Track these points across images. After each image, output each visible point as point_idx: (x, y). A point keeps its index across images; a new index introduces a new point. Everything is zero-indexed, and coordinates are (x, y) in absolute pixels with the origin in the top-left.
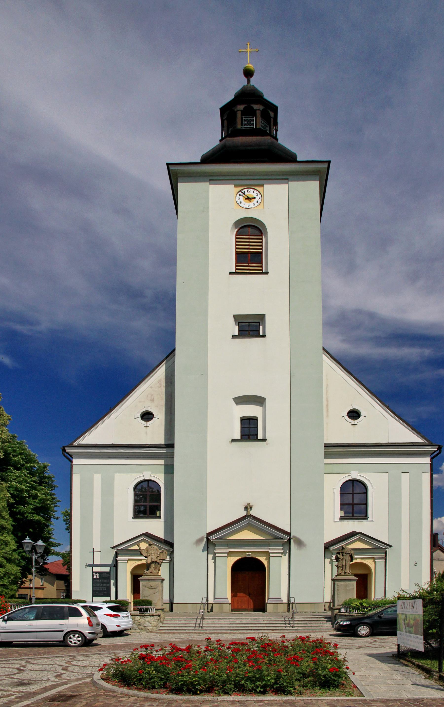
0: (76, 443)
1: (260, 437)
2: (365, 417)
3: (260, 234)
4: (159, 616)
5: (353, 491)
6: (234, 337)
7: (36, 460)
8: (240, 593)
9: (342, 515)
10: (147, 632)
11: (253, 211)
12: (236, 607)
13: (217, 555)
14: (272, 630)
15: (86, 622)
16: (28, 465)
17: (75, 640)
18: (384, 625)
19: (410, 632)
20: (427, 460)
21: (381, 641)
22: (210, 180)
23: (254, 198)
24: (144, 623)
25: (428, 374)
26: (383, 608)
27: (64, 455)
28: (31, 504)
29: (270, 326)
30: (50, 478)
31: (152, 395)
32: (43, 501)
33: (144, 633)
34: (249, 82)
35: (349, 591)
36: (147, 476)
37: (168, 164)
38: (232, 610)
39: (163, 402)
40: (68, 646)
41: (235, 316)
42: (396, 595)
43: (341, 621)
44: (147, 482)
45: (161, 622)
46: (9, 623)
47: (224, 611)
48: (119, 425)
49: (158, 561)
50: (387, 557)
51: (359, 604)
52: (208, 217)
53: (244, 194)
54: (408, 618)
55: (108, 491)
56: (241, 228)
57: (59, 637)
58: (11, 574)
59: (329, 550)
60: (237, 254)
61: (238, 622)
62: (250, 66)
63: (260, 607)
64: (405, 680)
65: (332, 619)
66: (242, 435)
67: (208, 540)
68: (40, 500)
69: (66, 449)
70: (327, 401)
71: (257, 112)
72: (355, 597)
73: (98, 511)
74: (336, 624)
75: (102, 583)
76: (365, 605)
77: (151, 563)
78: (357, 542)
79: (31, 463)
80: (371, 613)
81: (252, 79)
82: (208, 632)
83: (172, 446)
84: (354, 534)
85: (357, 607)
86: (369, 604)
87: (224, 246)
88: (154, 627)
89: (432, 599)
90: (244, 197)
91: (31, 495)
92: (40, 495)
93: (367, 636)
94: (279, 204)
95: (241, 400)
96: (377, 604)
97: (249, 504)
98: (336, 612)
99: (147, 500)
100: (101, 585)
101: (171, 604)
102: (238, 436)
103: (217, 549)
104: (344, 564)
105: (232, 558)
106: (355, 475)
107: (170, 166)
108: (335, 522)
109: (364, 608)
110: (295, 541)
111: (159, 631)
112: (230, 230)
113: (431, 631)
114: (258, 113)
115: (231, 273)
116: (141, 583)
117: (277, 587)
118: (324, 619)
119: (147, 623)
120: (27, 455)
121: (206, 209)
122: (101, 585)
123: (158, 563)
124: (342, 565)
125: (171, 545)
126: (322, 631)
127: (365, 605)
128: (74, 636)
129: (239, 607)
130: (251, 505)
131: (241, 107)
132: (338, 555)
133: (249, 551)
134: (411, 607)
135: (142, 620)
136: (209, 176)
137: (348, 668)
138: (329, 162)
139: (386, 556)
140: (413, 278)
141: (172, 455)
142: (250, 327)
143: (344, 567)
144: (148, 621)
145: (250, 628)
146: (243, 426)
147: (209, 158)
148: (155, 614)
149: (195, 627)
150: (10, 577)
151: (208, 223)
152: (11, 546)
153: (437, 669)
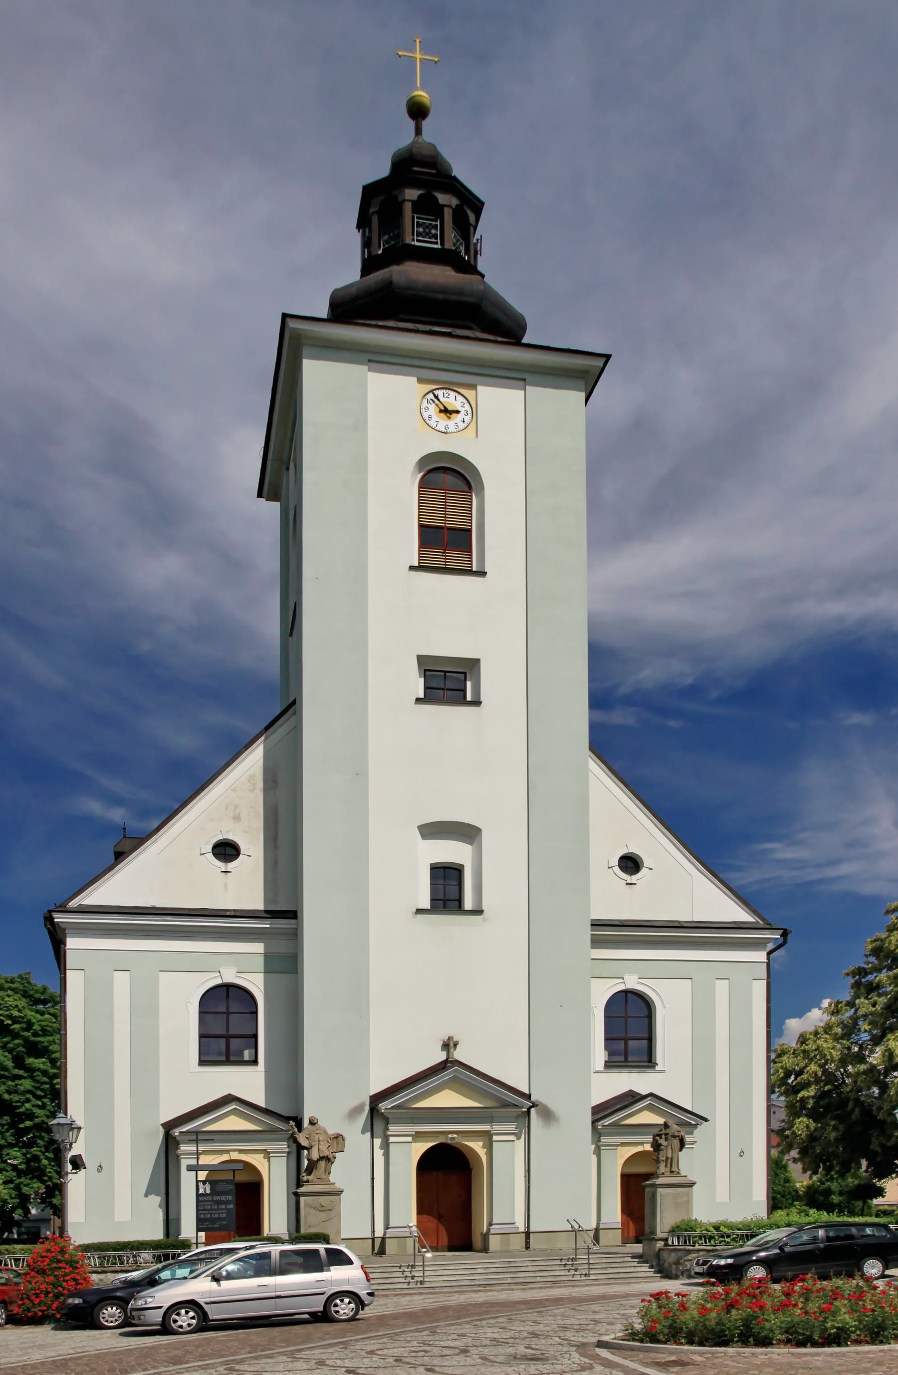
0: (73, 904)
1: (468, 905)
2: (651, 869)
3: (467, 490)
6: (418, 701)
13: (392, 1139)
14: (554, 1282)
22: (370, 361)
23: (458, 412)
31: (236, 807)
34: (418, 131)
36: (230, 976)
37: (285, 316)
39: (259, 823)
41: (421, 659)
46: (224, 1284)
48: (167, 868)
53: (438, 400)
55: (146, 1009)
56: (430, 472)
57: (317, 1305)
60: (421, 527)
62: (422, 95)
67: (373, 1110)
69: (55, 915)
71: (446, 209)
73: (130, 1052)
75: (218, 1203)
76: (725, 1230)
81: (425, 124)
82: (437, 1290)
83: (293, 915)
84: (630, 1099)
85: (709, 1234)
87: (396, 512)
90: (437, 405)
94: (506, 429)
95: (433, 830)
97: (450, 1038)
98: (660, 1244)
99: (226, 1026)
100: (216, 1207)
102: (425, 903)
104: (670, 1155)
105: (419, 1145)
106: (632, 982)
109: (722, 1236)
110: (537, 1113)
114: (448, 214)
117: (504, 1202)
121: (360, 425)
122: (216, 1207)
124: (667, 1158)
126: (641, 1280)
127: (725, 1230)
128: (342, 1301)
130: (455, 1039)
131: (412, 194)
132: (658, 1138)
138: (608, 357)
141: (296, 935)
142: (448, 682)
143: (669, 1161)
145: (509, 1281)
147: (347, 308)
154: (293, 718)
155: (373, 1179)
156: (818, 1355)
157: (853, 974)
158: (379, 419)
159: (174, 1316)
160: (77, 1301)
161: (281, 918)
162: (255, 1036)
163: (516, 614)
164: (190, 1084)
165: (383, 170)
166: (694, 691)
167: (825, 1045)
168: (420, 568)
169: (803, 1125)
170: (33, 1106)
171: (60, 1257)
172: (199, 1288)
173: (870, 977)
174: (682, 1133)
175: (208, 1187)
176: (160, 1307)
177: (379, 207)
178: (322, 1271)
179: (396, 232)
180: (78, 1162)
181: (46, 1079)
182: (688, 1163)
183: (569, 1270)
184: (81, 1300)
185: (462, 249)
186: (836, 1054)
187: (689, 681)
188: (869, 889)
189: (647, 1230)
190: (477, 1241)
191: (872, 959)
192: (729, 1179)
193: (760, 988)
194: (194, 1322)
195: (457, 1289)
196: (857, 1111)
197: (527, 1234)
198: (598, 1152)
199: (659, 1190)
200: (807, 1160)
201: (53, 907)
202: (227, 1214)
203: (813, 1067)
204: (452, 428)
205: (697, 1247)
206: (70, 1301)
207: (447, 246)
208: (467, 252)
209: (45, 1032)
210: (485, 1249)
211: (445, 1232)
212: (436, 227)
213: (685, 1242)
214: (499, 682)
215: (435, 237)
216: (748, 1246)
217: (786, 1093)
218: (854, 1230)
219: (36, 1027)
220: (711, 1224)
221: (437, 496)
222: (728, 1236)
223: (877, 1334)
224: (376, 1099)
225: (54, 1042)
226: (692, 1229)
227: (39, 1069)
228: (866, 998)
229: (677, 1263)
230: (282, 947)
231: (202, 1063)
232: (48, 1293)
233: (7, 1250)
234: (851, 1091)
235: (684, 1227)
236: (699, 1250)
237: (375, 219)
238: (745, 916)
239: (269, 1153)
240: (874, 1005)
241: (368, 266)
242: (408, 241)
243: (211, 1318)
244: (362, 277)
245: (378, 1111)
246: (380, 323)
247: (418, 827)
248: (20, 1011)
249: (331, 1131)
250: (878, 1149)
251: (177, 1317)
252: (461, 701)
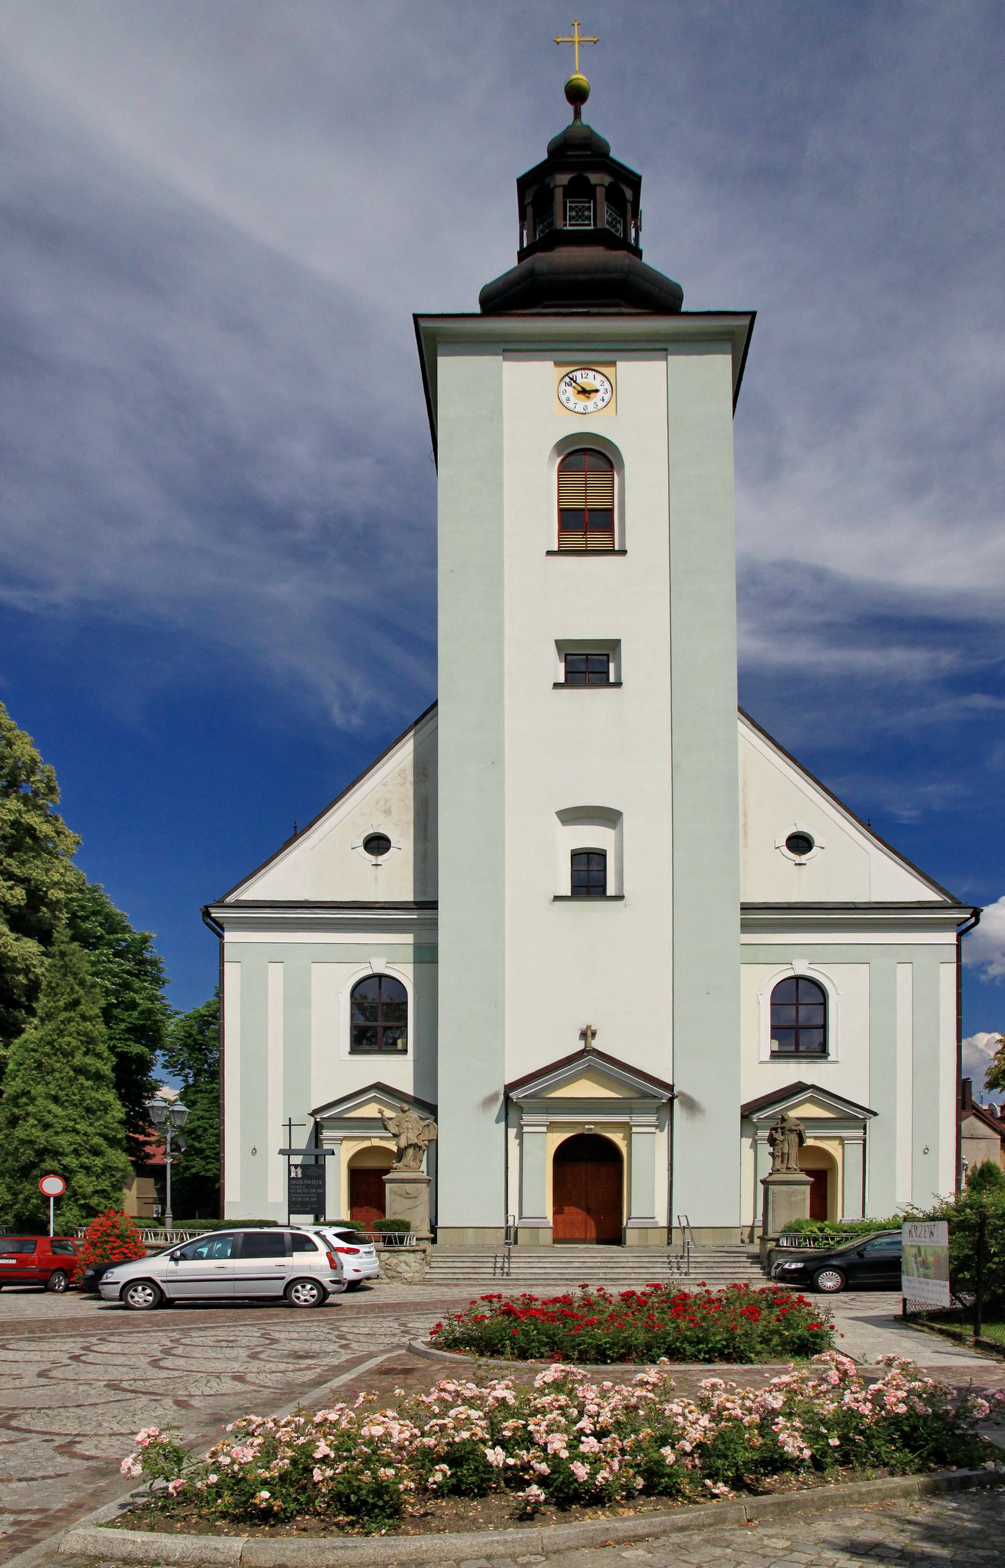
0: (230, 899)
1: (611, 891)
4: (424, 1251)
5: (797, 1000)
6: (557, 686)
7: (126, 926)
8: (569, 1205)
9: (777, 1049)
10: (403, 1283)
11: (595, 420)
12: (561, 1235)
15: (326, 1261)
16: (111, 937)
17: (306, 1294)
18: (872, 1268)
19: (926, 1276)
20: (951, 937)
21: (864, 1299)
22: (504, 351)
23: (597, 391)
24: (397, 1265)
25: (947, 709)
26: (867, 1238)
27: (207, 924)
28: (123, 1021)
29: (630, 664)
30: (154, 963)
32: (149, 1013)
33: (396, 1284)
34: (577, 114)
35: (796, 1205)
36: (379, 967)
37: (416, 317)
38: (556, 1240)
39: (410, 816)
40: (293, 1306)
41: (560, 644)
42: (902, 1214)
43: (786, 1262)
44: (377, 979)
45: (428, 1264)
46: (183, 1264)
49: (420, 1144)
50: (867, 1136)
51: (816, 1230)
52: (500, 431)
53: (575, 382)
54: (923, 1253)
55: (298, 999)
57: (277, 1289)
58: (117, 1169)
59: (751, 1120)
60: (561, 511)
61: (577, 1265)
62: (581, 78)
63: (612, 1233)
64: (920, 1347)
65: (763, 1260)
66: (574, 887)
67: (507, 1099)
68: (142, 1012)
69: (211, 910)
70: (745, 815)
71: (598, 189)
72: (807, 1216)
74: (776, 1268)
75: (307, 1186)
77: (406, 1148)
78: (808, 1104)
79: (117, 933)
80: (841, 1247)
81: (584, 108)
83: (433, 905)
84: (799, 1088)
86: (836, 1230)
87: (534, 495)
88: (416, 1275)
89: (962, 1221)
91: (123, 1001)
92: (141, 1001)
93: (837, 1291)
94: (646, 401)
95: (572, 816)
96: (852, 1231)
97: (589, 1027)
98: (771, 1245)
99: (378, 1018)
101: (434, 1229)
102: (565, 889)
103: (527, 1118)
104: (786, 1151)
105: (556, 1135)
106: (801, 968)
107: (419, 320)
108: (762, 1062)
109: (827, 1239)
110: (682, 1103)
111: (426, 1282)
113: (960, 1276)
114: (600, 193)
115: (549, 553)
116: (388, 1186)
117: (645, 1198)
118: (745, 1259)
119: (403, 1265)
120: (108, 916)
121: (496, 415)
123: (420, 1147)
124: (783, 1153)
125: (431, 1109)
128: (303, 1287)
129: (568, 1236)
131: (563, 179)
133: (589, 1122)
134: (928, 1234)
135: (393, 1261)
136: (497, 342)
137: (832, 1327)
138: (753, 314)
139: (865, 1134)
140: (915, 487)
141: (433, 925)
142: (589, 665)
143: (786, 1157)
144: (405, 1262)
145: (601, 1276)
146: (575, 868)
147: (498, 300)
148: (417, 1248)
149: (495, 1274)
150: (113, 1176)
151: (500, 447)
152: (115, 1114)
153: (972, 1333)
158: (520, 406)
164: (341, 1070)
168: (560, 552)
174: (801, 1128)
175: (299, 1171)
176: (117, 1283)
195: (541, 1282)
197: (670, 1229)
204: (591, 408)
215: (588, 218)
221: (576, 478)
224: (510, 1088)
238: (930, 895)
242: (559, 225)
246: (520, 312)
247: (557, 813)
251: (134, 1294)
252: (608, 684)
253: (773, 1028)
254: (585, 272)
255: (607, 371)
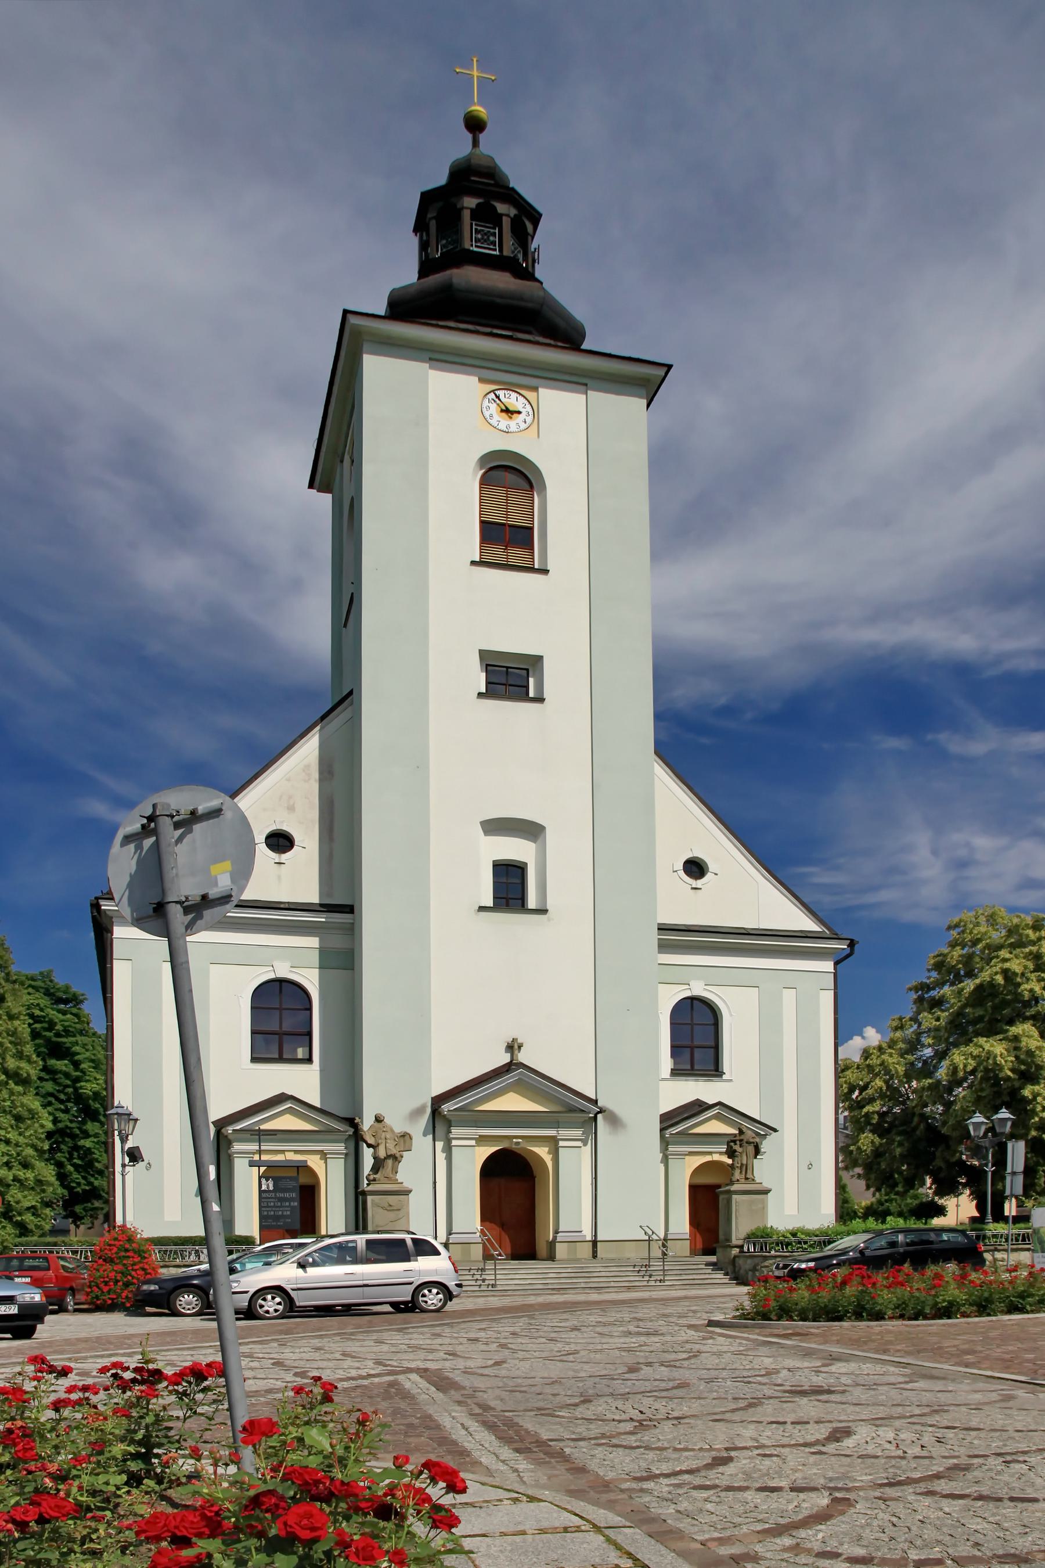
1: (532, 903)
3: (528, 488)
20: (828, 966)
22: (431, 359)
23: (519, 413)
31: (290, 797)
34: (475, 143)
36: (283, 971)
37: (346, 312)
39: (315, 814)
40: (423, 1311)
41: (483, 654)
46: (312, 1271)
47: (473, 1259)
57: (404, 1295)
60: (482, 522)
62: (479, 110)
67: (435, 1112)
69: (102, 902)
71: (504, 218)
75: (281, 1200)
81: (482, 137)
82: (509, 1293)
83: (349, 909)
84: (697, 1108)
87: (456, 508)
94: (562, 428)
95: (495, 827)
98: (735, 1251)
99: (280, 1020)
104: (744, 1162)
106: (698, 989)
109: (800, 1243)
110: (605, 1118)
112: (471, 470)
114: (506, 223)
115: (473, 563)
121: (421, 421)
127: (803, 1236)
128: (430, 1291)
130: (519, 1041)
131: (470, 202)
136: (427, 350)
138: (669, 367)
141: (353, 931)
142: (510, 678)
145: (583, 1285)
147: (403, 307)
150: (44, 1191)
154: (349, 710)
155: (435, 1183)
156: (931, 1325)
157: (916, 989)
158: (436, 416)
159: (260, 1301)
160: (153, 1287)
161: (338, 912)
162: (309, 1034)
163: (589, 608)
165: (441, 179)
166: (728, 711)
167: (891, 1060)
169: (867, 1140)
170: (56, 1110)
171: (128, 1246)
172: (285, 1273)
173: (933, 993)
175: (271, 1183)
176: (246, 1292)
177: (436, 214)
178: (409, 1260)
179: (454, 237)
180: (136, 1154)
181: (69, 1082)
182: (762, 1170)
183: (643, 1276)
184: (157, 1287)
185: (520, 257)
186: (901, 1069)
187: (723, 701)
188: (908, 916)
189: (721, 1237)
190: (542, 1248)
191: (934, 974)
192: (800, 1189)
193: (827, 999)
194: (280, 1308)
195: (530, 1292)
196: (922, 1126)
197: (595, 1243)
198: (665, 1160)
199: (734, 1197)
200: (873, 1176)
201: (99, 894)
202: (291, 1211)
203: (879, 1083)
204: (513, 427)
205: (773, 1252)
206: (145, 1287)
207: (505, 253)
208: (525, 259)
209: (67, 1032)
210: (551, 1257)
211: (508, 1240)
212: (494, 235)
213: (762, 1249)
214: (563, 678)
216: (828, 1250)
217: (851, 1108)
218: (932, 1236)
219: (59, 1027)
220: (787, 1231)
222: (806, 1243)
223: (985, 1307)
224: (438, 1101)
225: (77, 1043)
226: (768, 1236)
227: (60, 1072)
228: (930, 1013)
229: (754, 1269)
230: (338, 942)
231: (254, 1059)
232: (117, 1281)
233: (63, 1242)
234: (916, 1106)
235: (759, 1234)
236: (776, 1257)
237: (433, 225)
239: (326, 1154)
240: (938, 1019)
241: (426, 268)
242: (467, 246)
243: (298, 1304)
244: (419, 279)
245: (440, 1113)
246: (441, 323)
247: (481, 823)
248: (41, 1010)
249: (398, 1129)
250: (942, 1165)
251: (263, 1303)
252: (525, 697)
253: (672, 1047)
254: (501, 296)
255: (531, 395)
